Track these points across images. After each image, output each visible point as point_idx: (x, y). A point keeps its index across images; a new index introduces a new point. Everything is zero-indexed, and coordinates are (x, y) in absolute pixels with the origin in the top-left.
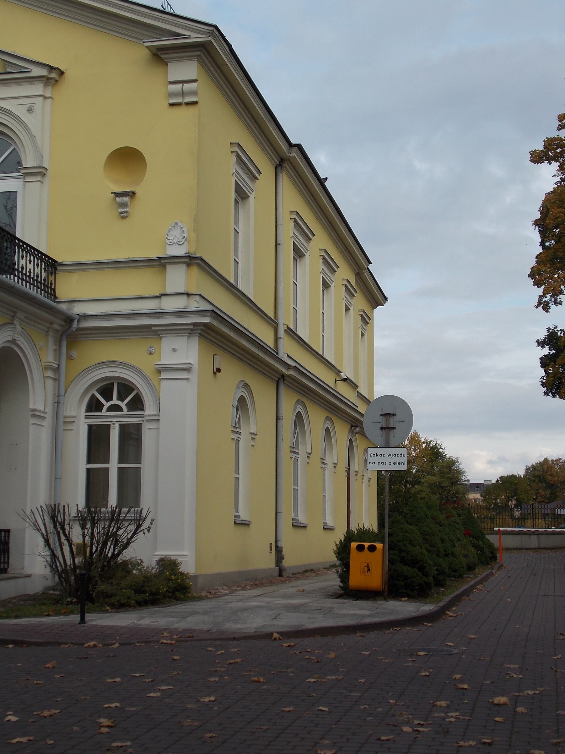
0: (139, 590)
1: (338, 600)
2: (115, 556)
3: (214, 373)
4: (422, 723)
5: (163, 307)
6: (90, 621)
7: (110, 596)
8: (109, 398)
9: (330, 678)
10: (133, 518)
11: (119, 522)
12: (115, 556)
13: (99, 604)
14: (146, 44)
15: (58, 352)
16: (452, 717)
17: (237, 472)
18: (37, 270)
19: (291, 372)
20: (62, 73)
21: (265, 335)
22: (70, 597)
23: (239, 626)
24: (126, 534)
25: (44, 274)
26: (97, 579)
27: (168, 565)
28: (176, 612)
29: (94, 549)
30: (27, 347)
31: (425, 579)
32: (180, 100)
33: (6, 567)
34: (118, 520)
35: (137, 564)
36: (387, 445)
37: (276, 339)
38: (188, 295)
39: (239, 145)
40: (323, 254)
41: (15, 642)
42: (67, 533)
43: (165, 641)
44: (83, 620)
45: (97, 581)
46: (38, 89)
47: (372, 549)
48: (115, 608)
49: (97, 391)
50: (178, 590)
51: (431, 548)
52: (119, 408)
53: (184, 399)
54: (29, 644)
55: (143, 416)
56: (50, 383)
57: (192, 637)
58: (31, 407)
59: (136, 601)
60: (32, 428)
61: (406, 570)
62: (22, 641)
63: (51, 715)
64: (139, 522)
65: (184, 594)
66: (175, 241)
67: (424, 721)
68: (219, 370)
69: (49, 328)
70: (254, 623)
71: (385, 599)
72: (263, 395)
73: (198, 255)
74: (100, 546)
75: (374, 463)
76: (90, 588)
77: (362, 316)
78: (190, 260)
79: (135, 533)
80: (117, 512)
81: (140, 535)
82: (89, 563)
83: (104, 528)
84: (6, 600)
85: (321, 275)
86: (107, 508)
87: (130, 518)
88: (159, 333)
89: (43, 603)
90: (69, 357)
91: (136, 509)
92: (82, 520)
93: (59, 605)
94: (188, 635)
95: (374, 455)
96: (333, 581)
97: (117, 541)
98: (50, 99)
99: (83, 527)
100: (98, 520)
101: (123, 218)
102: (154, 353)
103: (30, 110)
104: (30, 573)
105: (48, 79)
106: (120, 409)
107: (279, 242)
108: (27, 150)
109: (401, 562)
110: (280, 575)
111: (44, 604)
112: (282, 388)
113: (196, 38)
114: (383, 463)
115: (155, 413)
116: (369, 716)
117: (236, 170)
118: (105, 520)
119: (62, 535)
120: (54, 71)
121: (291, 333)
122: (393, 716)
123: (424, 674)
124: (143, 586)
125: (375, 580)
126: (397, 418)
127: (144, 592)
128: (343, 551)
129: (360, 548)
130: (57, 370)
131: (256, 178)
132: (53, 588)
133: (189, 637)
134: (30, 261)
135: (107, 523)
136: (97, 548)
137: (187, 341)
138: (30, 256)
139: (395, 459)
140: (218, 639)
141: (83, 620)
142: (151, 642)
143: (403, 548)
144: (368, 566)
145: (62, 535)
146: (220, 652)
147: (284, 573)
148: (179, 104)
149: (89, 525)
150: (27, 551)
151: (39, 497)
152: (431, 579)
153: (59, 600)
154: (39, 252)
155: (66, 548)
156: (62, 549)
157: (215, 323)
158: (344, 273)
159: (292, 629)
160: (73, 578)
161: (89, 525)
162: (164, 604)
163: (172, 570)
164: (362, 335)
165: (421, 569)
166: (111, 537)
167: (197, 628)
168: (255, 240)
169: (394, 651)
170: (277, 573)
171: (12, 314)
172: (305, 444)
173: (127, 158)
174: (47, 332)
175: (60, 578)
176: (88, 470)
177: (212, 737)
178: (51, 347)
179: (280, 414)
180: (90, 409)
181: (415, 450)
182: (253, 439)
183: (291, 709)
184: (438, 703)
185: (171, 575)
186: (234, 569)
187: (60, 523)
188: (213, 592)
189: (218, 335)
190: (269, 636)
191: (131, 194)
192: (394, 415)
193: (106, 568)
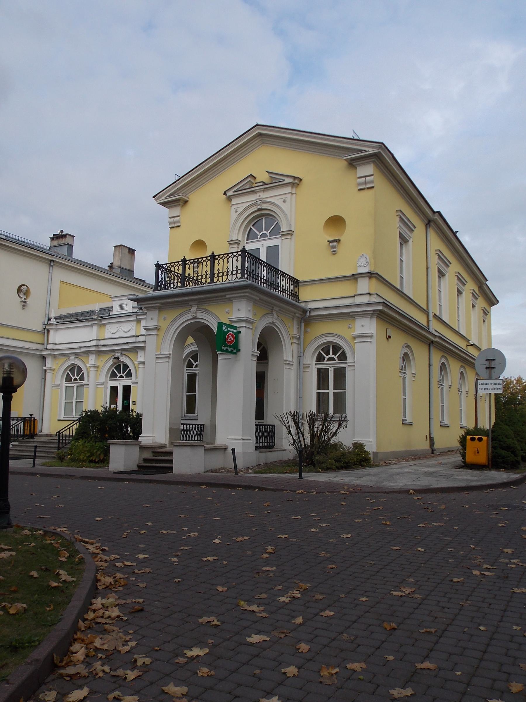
0: (338, 460)
1: (460, 470)
3: (387, 339)
4: (489, 567)
5: (356, 302)
8: (328, 353)
9: (435, 524)
12: (329, 440)
15: (299, 329)
16: (514, 563)
17: (404, 394)
18: (287, 285)
19: (437, 339)
20: (301, 180)
21: (421, 319)
23: (391, 484)
27: (359, 446)
31: (516, 458)
36: (490, 378)
37: (428, 321)
38: (370, 294)
39: (401, 211)
40: (457, 274)
41: (260, 489)
43: (343, 492)
46: (288, 189)
47: (480, 440)
51: (522, 440)
52: (333, 359)
53: (369, 353)
54: (266, 489)
55: (346, 363)
56: (295, 346)
61: (503, 452)
63: (241, 541)
66: (362, 265)
67: (491, 566)
68: (390, 337)
70: (401, 483)
71: (490, 470)
72: (420, 353)
73: (376, 272)
75: (482, 389)
77: (483, 311)
78: (371, 275)
79: (338, 428)
84: (272, 463)
85: (456, 286)
90: (305, 332)
95: (482, 384)
96: (458, 458)
105: (294, 184)
106: (334, 360)
109: (500, 448)
110: (433, 453)
112: (432, 348)
113: (372, 151)
114: (487, 389)
115: (353, 361)
116: (452, 558)
121: (438, 318)
122: (470, 559)
123: (501, 525)
125: (482, 458)
126: (496, 362)
127: (341, 462)
128: (463, 441)
129: (473, 439)
130: (299, 339)
131: (413, 231)
139: (495, 386)
140: (377, 492)
143: (502, 440)
144: (478, 450)
147: (435, 452)
148: (174, 227)
152: (520, 458)
157: (386, 310)
158: (471, 285)
159: (424, 488)
164: (484, 321)
165: (514, 452)
168: (413, 267)
169: (486, 505)
170: (431, 452)
171: (271, 308)
172: (447, 380)
173: (336, 222)
176: (319, 394)
177: (332, 568)
178: (296, 326)
179: (431, 363)
181: (519, 386)
183: (398, 548)
184: (505, 550)
186: (404, 449)
188: (387, 462)
189: (388, 317)
190: (407, 491)
192: (494, 360)
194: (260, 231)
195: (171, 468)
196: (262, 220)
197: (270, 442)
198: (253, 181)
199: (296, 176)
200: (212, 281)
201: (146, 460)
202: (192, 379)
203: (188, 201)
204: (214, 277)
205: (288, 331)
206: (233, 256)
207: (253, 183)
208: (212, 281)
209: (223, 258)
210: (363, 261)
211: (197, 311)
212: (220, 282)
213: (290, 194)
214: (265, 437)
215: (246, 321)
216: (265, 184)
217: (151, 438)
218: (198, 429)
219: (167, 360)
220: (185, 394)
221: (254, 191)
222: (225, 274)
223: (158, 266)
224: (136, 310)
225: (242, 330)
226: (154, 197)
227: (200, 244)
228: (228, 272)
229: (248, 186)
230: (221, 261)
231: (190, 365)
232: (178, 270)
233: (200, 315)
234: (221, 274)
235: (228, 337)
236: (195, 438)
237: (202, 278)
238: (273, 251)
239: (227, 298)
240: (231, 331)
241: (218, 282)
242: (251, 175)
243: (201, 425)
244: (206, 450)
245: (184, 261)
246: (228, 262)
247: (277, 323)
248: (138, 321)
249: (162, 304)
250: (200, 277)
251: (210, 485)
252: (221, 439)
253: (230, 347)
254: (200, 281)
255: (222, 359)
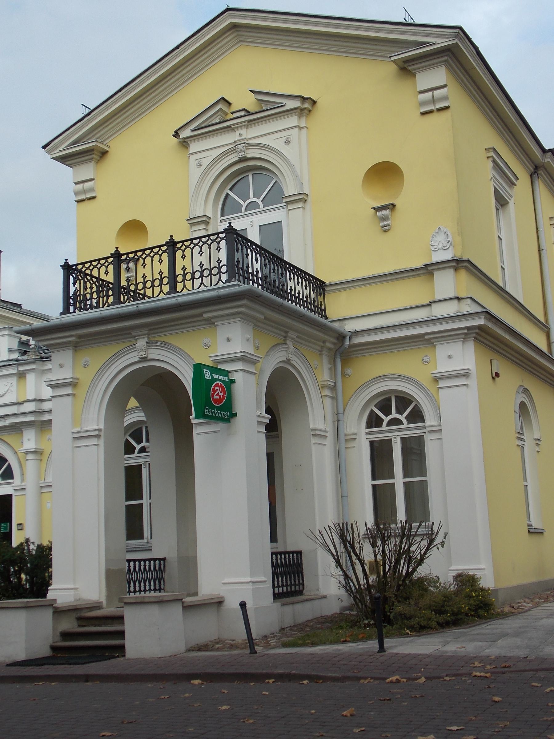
0: (440, 611)
2: (409, 574)
3: (493, 378)
6: (392, 647)
7: (409, 618)
8: (387, 412)
10: (425, 532)
11: (411, 538)
12: (409, 574)
13: (398, 626)
14: (392, 59)
15: (333, 370)
18: (306, 292)
20: (314, 102)
22: (367, 619)
24: (419, 551)
25: (313, 296)
26: (393, 600)
27: (467, 581)
28: (484, 634)
29: (387, 568)
30: (301, 364)
32: (431, 107)
33: (301, 588)
34: (409, 536)
35: (435, 581)
38: (459, 299)
42: (358, 552)
43: (478, 674)
44: (382, 648)
45: (394, 602)
46: (293, 121)
48: (415, 631)
49: (375, 406)
50: (480, 608)
52: (399, 422)
53: (463, 405)
55: (424, 427)
56: (328, 402)
57: (509, 667)
58: (312, 426)
59: (437, 622)
60: (314, 448)
62: (317, 676)
64: (431, 538)
65: (487, 611)
66: (440, 246)
69: (322, 347)
73: (465, 258)
74: (392, 565)
76: (387, 608)
78: (458, 264)
79: (428, 549)
80: (407, 527)
81: (434, 551)
82: (383, 583)
83: (395, 545)
84: (303, 623)
86: (396, 524)
87: (422, 533)
88: (432, 341)
89: (341, 626)
91: (427, 524)
92: (372, 538)
93: (356, 627)
94: (503, 665)
97: (410, 558)
98: (306, 129)
99: (374, 545)
100: (388, 537)
101: (385, 231)
102: (429, 362)
103: (287, 142)
104: (325, 594)
105: (302, 110)
107: (542, 247)
108: (287, 179)
111: (341, 628)
113: (441, 43)
115: (436, 423)
117: (494, 176)
118: (395, 536)
119: (353, 555)
120: (307, 101)
124: (443, 606)
127: (445, 612)
130: (334, 388)
131: (514, 184)
132: (350, 608)
133: (505, 667)
134: (298, 283)
135: (398, 540)
136: (390, 566)
137: (463, 345)
138: (298, 278)
141: (382, 648)
142: (461, 675)
145: (353, 555)
146: (549, 689)
148: (431, 112)
149: (379, 543)
150: (320, 572)
151: (327, 516)
153: (357, 622)
154: (306, 273)
155: (358, 568)
156: (354, 569)
157: (490, 325)
160: (368, 598)
161: (379, 543)
162: (468, 624)
163: (472, 586)
166: (403, 554)
167: (512, 655)
171: (283, 334)
173: (384, 173)
174: (321, 351)
175: (355, 600)
176: (374, 486)
178: (326, 366)
180: (369, 425)
182: (538, 445)
185: (471, 591)
187: (349, 542)
188: (516, 606)
189: (492, 338)
191: (391, 206)
193: (401, 588)
194: (245, 197)
195: (122, 648)
196: (246, 174)
197: (295, 585)
198: (225, 109)
199: (305, 96)
200: (173, 289)
201: (66, 635)
202: (133, 476)
203: (107, 152)
204: (175, 281)
205: (314, 374)
206: (152, 254)
207: (226, 114)
208: (173, 289)
209: (99, 266)
210: (440, 240)
211: (148, 347)
212: (189, 291)
213: (297, 129)
214: (288, 573)
215: (243, 359)
216: (248, 113)
217: (72, 592)
218: (155, 568)
219: (94, 441)
220: (145, 501)
221: (229, 127)
222: (157, 283)
223: (67, 268)
224: (15, 356)
225: (238, 377)
226: (44, 147)
227: (134, 227)
228: (202, 272)
229: (218, 118)
230: (148, 259)
231: (129, 449)
232: (107, 273)
233: (154, 353)
234: (189, 277)
235: (215, 391)
236: (150, 585)
237: (144, 287)
238: (273, 230)
239: (205, 320)
240: (218, 380)
241: (203, 288)
242: (223, 99)
243: (160, 560)
244: (187, 608)
245: (117, 256)
246: (144, 265)
247: (296, 361)
248: (21, 376)
249: (80, 337)
250: (140, 286)
251: (209, 677)
252: (207, 587)
253: (219, 409)
254: (142, 292)
255: (202, 435)
